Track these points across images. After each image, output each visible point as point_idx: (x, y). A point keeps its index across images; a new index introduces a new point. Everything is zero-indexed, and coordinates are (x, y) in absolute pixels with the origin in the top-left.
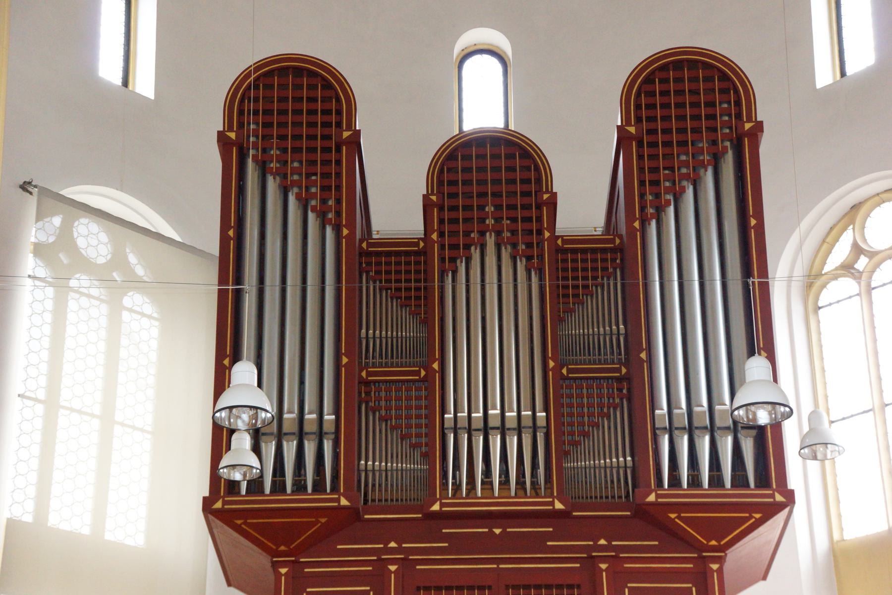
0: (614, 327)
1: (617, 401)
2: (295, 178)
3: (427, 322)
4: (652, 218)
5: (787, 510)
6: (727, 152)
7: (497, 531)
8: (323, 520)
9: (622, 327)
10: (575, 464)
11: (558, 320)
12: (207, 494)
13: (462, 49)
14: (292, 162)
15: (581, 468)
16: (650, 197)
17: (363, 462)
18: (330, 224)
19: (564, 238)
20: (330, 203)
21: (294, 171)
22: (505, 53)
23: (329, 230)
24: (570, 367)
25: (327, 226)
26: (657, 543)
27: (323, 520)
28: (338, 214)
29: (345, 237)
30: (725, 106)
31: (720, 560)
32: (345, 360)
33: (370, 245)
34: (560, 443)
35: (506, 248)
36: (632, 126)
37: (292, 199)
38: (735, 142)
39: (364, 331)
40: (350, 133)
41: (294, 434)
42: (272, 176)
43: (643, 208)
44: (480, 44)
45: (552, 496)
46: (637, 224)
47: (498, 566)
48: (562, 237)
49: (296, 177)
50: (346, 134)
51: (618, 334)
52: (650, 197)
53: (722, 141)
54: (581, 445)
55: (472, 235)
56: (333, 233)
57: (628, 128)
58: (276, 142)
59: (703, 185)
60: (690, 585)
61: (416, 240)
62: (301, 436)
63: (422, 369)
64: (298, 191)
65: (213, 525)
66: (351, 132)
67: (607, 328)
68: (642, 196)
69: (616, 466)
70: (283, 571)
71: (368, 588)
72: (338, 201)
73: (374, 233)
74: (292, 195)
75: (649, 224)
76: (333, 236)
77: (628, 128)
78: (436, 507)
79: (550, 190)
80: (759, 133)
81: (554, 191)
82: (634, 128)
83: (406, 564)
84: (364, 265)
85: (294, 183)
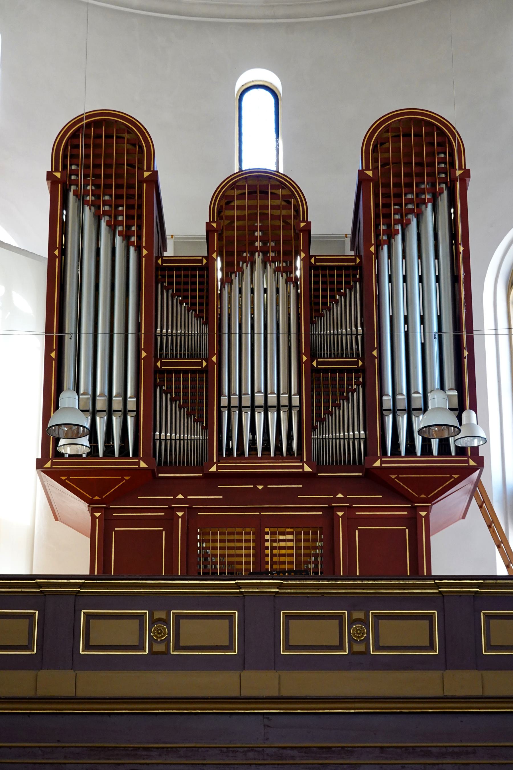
0: (354, 329)
1: (355, 387)
2: (106, 209)
3: (207, 322)
4: (384, 244)
5: (478, 471)
6: (443, 193)
7: (260, 487)
8: (127, 478)
9: (360, 328)
10: (321, 436)
11: (311, 323)
12: (40, 457)
13: (242, 85)
14: (104, 195)
15: (318, 439)
16: (383, 227)
17: (158, 433)
18: (133, 245)
19: (317, 257)
20: (133, 228)
21: (105, 203)
22: (277, 88)
23: (132, 249)
24: (318, 360)
25: (131, 247)
26: (381, 496)
27: (127, 478)
28: (140, 237)
29: (145, 257)
30: (442, 155)
31: (427, 509)
32: (144, 354)
33: (164, 261)
34: (310, 420)
35: (270, 266)
36: (370, 170)
37: (103, 224)
38: (449, 185)
39: (159, 330)
40: (150, 173)
41: (104, 411)
42: (89, 207)
43: (377, 235)
44: (256, 81)
45: (302, 461)
46: (372, 249)
47: (260, 513)
48: (315, 256)
49: (107, 208)
50: (146, 174)
51: (357, 334)
52: (383, 227)
53: (439, 184)
54: (326, 421)
55: (244, 255)
56: (135, 253)
57: (367, 172)
58: (92, 179)
59: (424, 217)
60: (405, 528)
61: (201, 258)
62: (110, 412)
63: (204, 361)
64: (108, 219)
65: (44, 479)
66: (150, 173)
67: (348, 330)
68: (377, 225)
69: (358, 437)
70: (97, 515)
71: (162, 529)
72: (140, 227)
73: (167, 237)
74: (104, 222)
75: (382, 249)
76: (136, 254)
77: (367, 172)
78: (213, 469)
79: (306, 220)
80: (467, 179)
81: (309, 221)
82: (372, 172)
83: (190, 511)
84: (160, 277)
85: (105, 213)
